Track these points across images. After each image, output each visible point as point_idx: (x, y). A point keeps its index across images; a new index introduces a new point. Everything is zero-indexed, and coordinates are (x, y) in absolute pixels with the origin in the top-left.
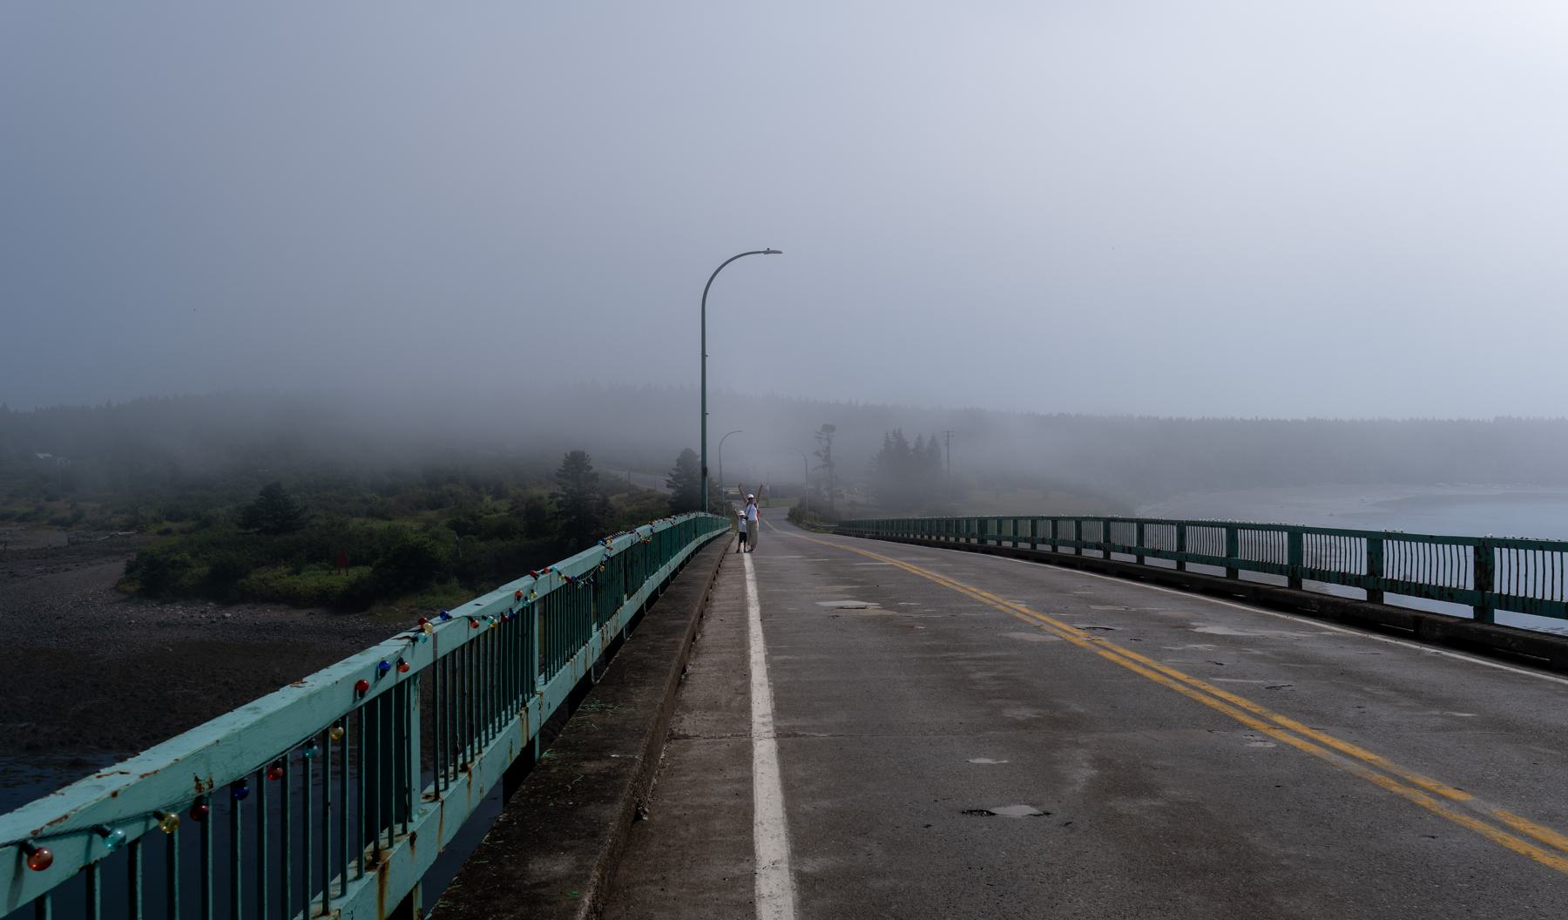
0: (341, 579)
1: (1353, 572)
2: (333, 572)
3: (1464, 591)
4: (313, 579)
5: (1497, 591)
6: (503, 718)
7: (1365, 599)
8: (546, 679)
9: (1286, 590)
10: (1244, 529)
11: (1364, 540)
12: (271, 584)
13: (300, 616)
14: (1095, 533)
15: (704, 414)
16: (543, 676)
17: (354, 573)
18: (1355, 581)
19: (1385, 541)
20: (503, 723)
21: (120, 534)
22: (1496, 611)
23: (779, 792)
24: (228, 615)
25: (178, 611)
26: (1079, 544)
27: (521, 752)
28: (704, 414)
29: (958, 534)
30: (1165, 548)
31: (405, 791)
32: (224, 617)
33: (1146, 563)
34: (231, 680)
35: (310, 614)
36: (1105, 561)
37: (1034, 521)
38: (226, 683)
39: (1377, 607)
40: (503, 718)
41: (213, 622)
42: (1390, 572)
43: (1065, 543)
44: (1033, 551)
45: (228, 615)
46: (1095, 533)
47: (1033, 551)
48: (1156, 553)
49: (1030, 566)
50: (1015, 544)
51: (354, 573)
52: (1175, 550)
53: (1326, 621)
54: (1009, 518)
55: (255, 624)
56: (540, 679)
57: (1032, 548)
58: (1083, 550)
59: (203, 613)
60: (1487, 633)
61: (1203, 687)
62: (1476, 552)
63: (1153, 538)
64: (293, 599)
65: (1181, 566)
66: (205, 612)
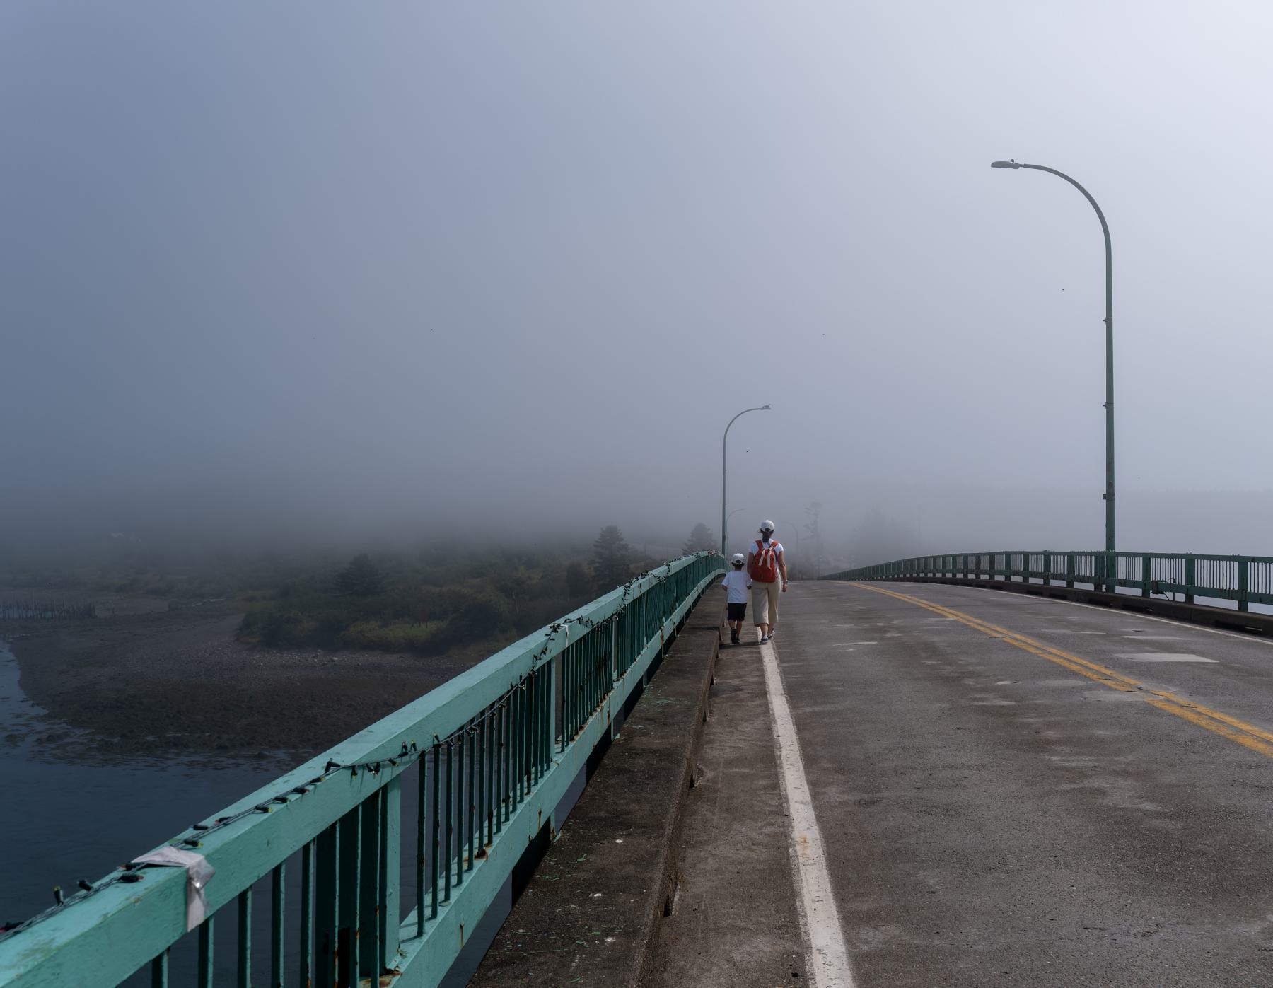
0: (423, 630)
1: (1256, 591)
2: (415, 625)
3: (1091, 577)
4: (399, 631)
5: (1196, 585)
6: (518, 792)
7: (1237, 609)
8: (563, 741)
9: (1184, 605)
10: (1266, 563)
11: (1236, 563)
12: (367, 635)
13: (392, 659)
14: (1037, 565)
15: (724, 470)
16: (413, 916)
17: (433, 626)
18: (1134, 584)
19: (1249, 563)
20: (518, 799)
21: (212, 600)
22: (1051, 581)
23: (846, 967)
24: (335, 659)
25: (293, 657)
26: (1047, 576)
27: (594, 750)
28: (724, 470)
29: (935, 571)
30: (1130, 578)
31: (374, 911)
32: (333, 661)
33: (1116, 592)
34: (353, 703)
35: (400, 657)
36: (1187, 605)
37: (1008, 555)
38: (350, 706)
39: (1192, 606)
40: (518, 792)
41: (325, 664)
42: (1252, 587)
43: (1035, 575)
44: (1242, 614)
45: (335, 659)
46: (1037, 565)
47: (1242, 614)
48: (1124, 583)
49: (1250, 644)
50: (1025, 579)
51: (433, 626)
52: (1093, 575)
53: (1268, 638)
54: (1001, 553)
55: (358, 665)
56: (555, 748)
57: (1024, 581)
58: (1196, 597)
59: (316, 657)
60: (1246, 618)
61: (1061, 660)
62: (1045, 557)
63: (1160, 572)
64: (384, 646)
65: (1243, 607)
66: (316, 657)
